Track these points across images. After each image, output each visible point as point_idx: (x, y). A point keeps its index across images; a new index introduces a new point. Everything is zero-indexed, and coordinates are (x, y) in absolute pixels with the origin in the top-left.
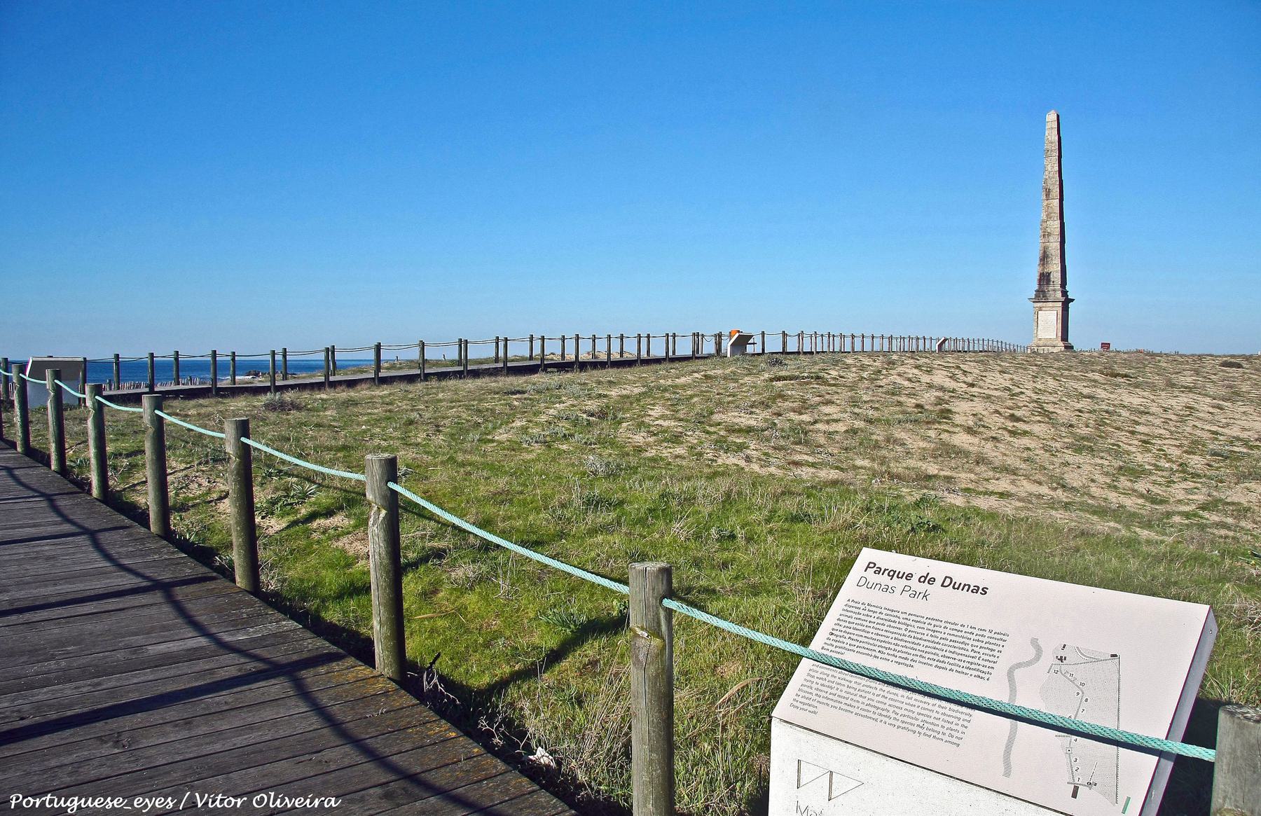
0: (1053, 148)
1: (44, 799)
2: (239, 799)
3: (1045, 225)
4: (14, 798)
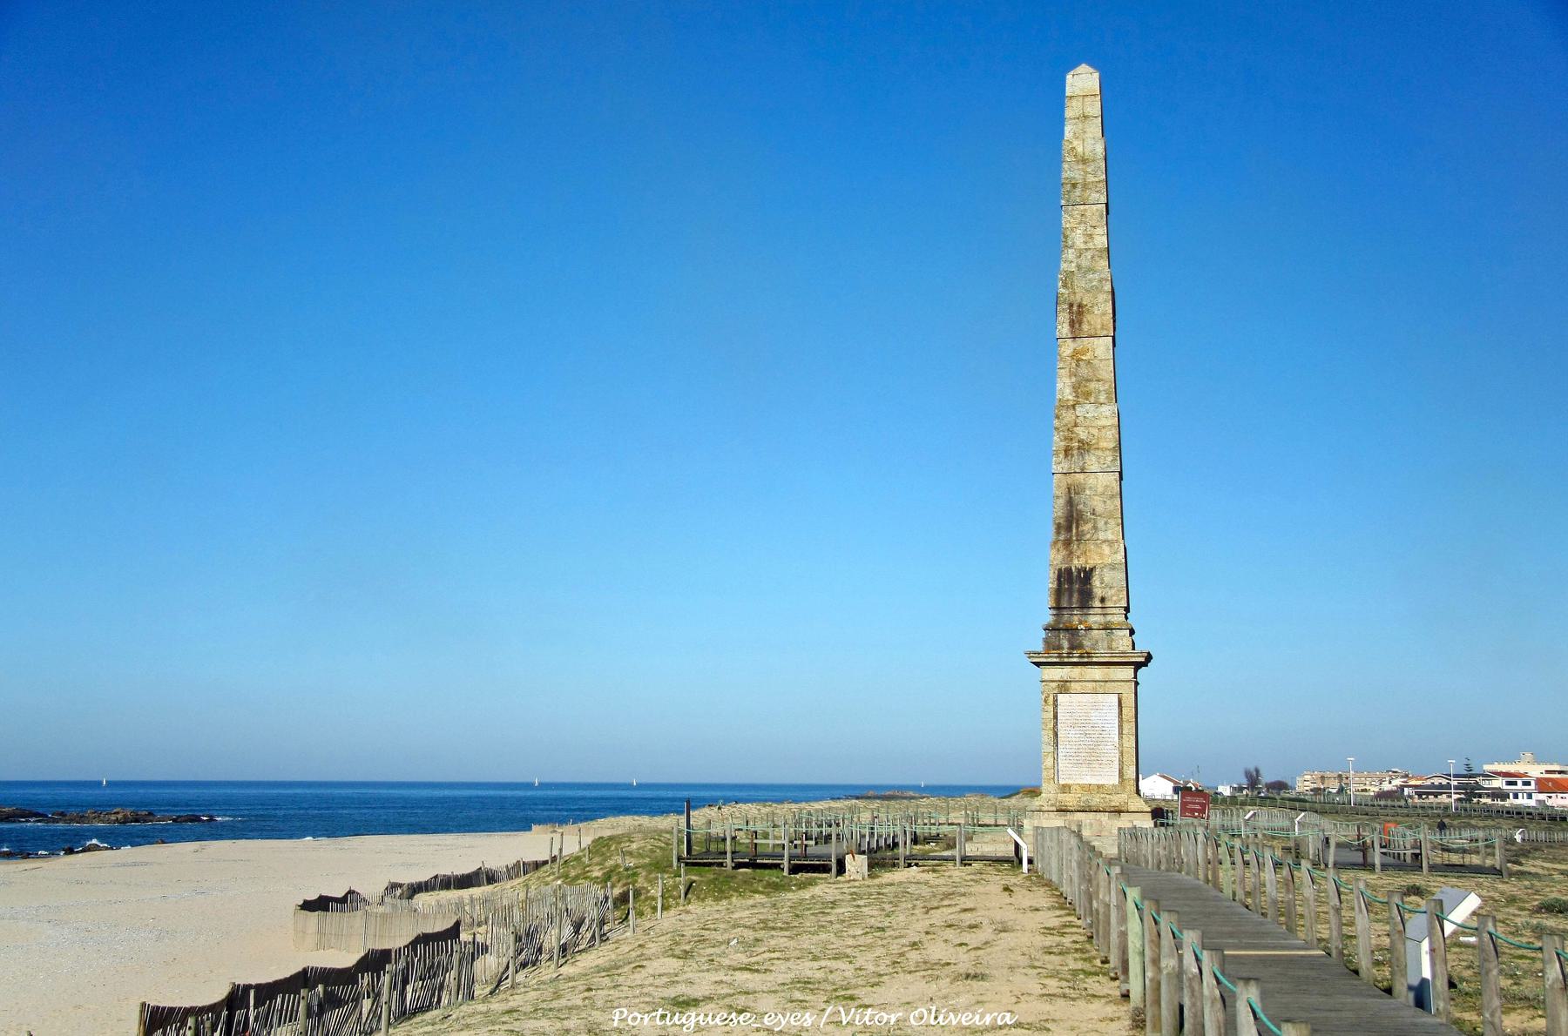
0: (1091, 178)
2: (893, 1015)
3: (1068, 417)
4: (618, 1014)
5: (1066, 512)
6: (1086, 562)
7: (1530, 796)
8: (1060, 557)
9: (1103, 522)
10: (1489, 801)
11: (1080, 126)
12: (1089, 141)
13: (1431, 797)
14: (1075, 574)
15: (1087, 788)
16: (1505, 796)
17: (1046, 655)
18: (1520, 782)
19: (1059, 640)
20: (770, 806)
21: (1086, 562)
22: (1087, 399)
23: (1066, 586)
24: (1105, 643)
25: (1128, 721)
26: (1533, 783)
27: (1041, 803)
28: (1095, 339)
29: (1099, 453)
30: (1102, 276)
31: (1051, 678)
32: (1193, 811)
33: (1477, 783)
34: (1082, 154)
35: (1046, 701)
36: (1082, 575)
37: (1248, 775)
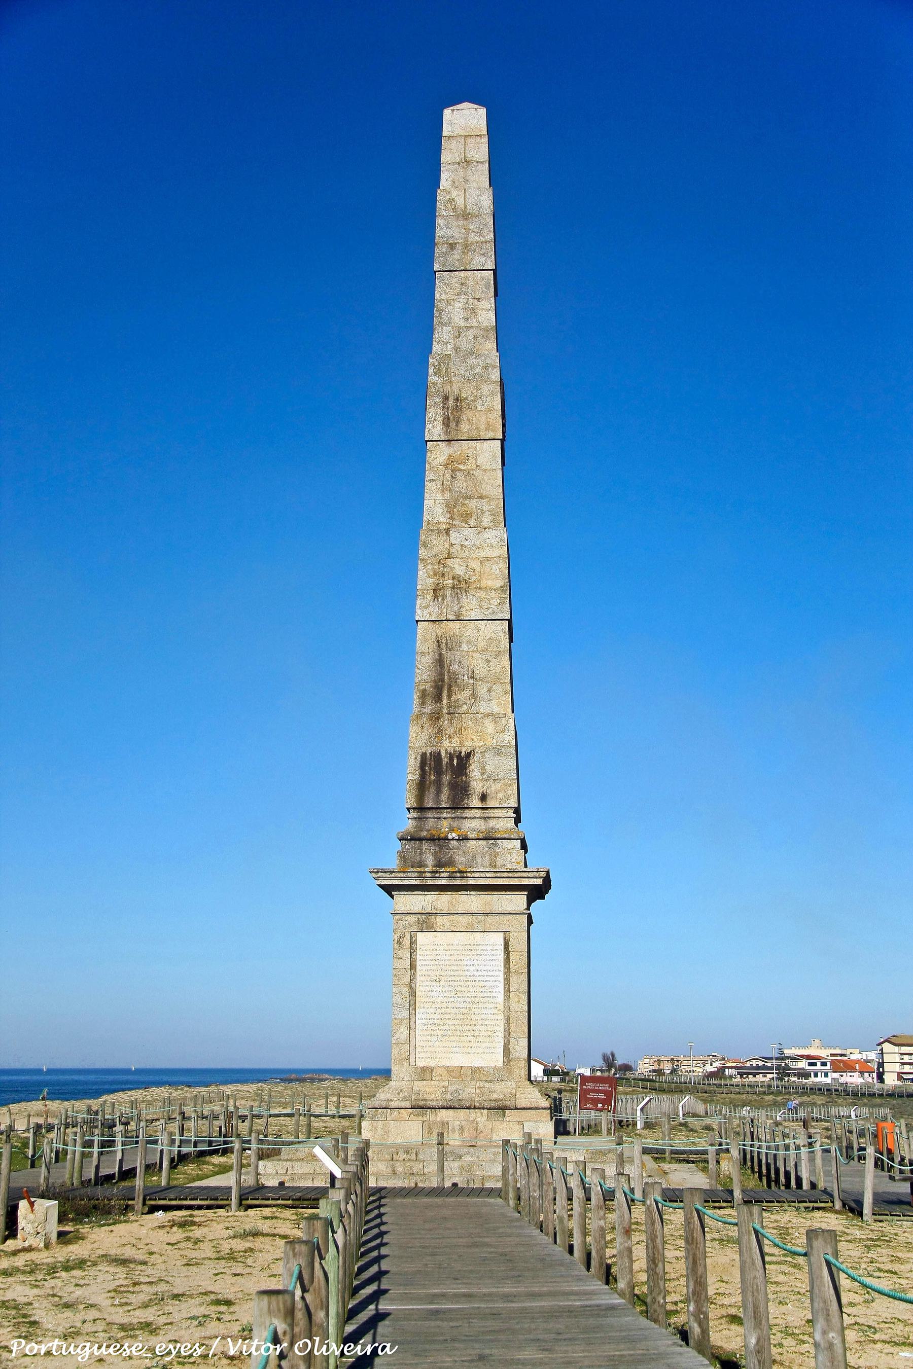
0: (474, 238)
1: (50, 1345)
4: (16, 1344)
5: (435, 674)
6: (461, 744)
7: (826, 1075)
8: (424, 737)
9: (485, 689)
10: (795, 1079)
11: (461, 173)
12: (472, 193)
13: (750, 1076)
14: (445, 761)
15: (457, 1073)
16: (807, 1075)
17: (402, 875)
18: (819, 1064)
19: (421, 854)
20: (182, 1089)
21: (461, 744)
22: (466, 522)
23: (433, 778)
24: (486, 860)
25: (517, 973)
26: (829, 1064)
27: (389, 1096)
28: (478, 443)
29: (482, 594)
30: (489, 361)
31: (407, 909)
32: (595, 1102)
33: (786, 1064)
34: (462, 206)
35: (399, 943)
36: (455, 762)
37: (605, 1058)
